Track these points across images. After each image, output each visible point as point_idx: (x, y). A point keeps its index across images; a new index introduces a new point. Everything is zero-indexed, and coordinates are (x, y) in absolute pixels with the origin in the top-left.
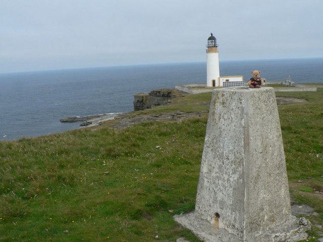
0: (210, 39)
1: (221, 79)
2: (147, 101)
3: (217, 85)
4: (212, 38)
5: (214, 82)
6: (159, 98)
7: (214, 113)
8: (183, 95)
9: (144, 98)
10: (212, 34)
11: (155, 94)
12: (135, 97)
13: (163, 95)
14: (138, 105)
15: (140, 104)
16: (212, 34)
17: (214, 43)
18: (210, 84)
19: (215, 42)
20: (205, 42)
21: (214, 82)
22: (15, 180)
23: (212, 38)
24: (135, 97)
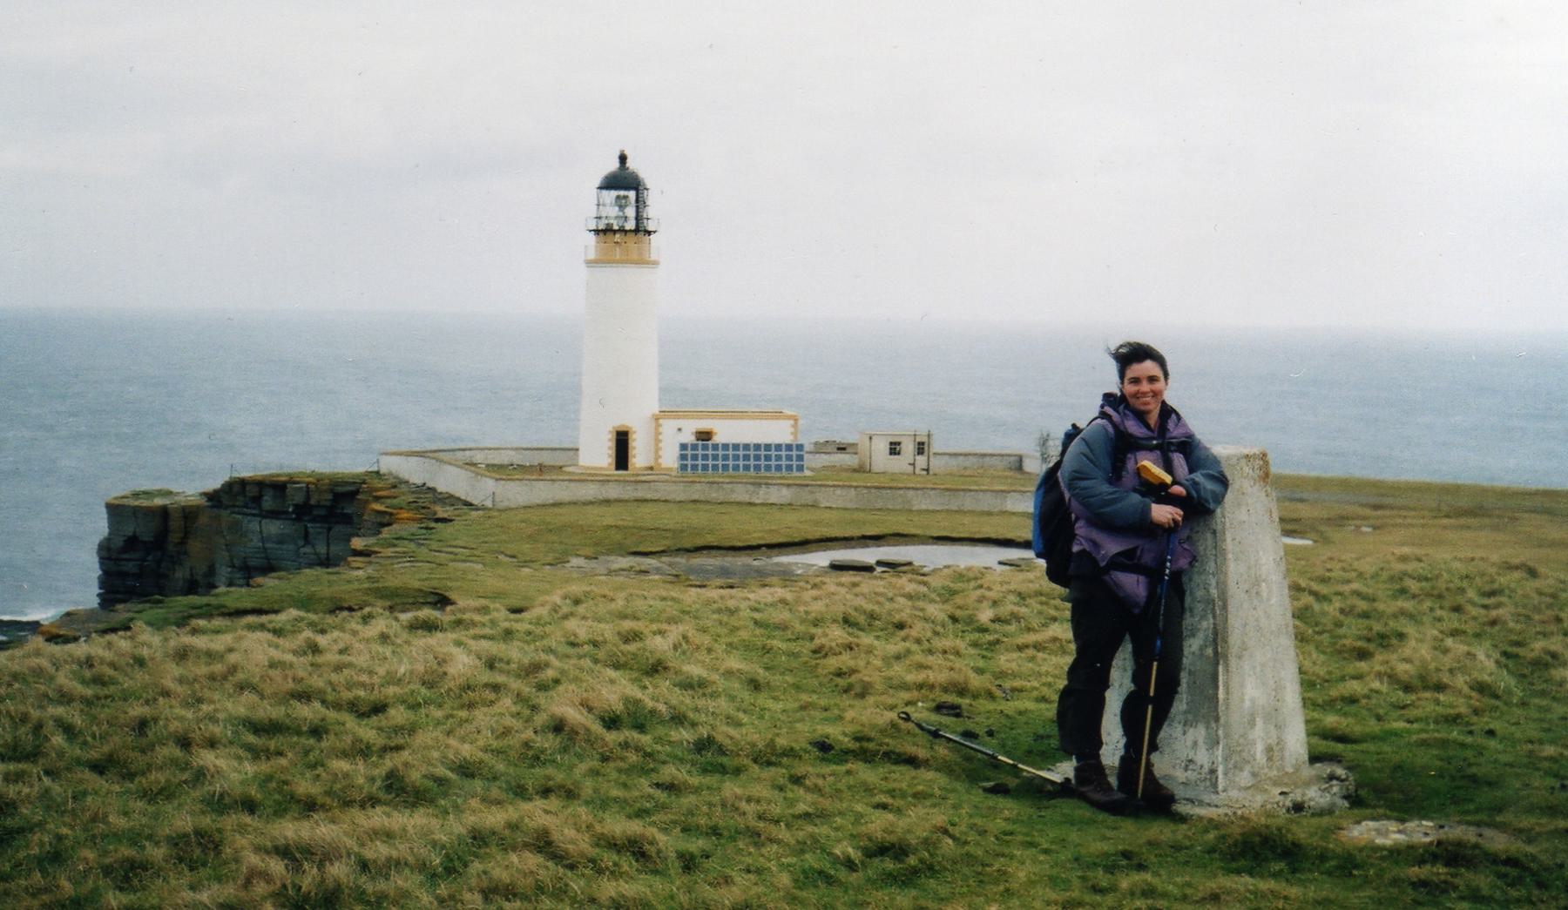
0: (611, 183)
1: (669, 426)
2: (195, 546)
3: (639, 457)
4: (622, 181)
5: (622, 441)
6: (273, 527)
7: (1267, 827)
8: (441, 512)
9: (176, 524)
10: (623, 159)
11: (245, 496)
12: (116, 511)
13: (303, 511)
14: (130, 567)
15: (155, 556)
16: (623, 159)
17: (631, 212)
18: (598, 455)
19: (640, 203)
20: (588, 203)
21: (622, 441)
22: (1322, 838)
23: (622, 181)
24: (116, 511)
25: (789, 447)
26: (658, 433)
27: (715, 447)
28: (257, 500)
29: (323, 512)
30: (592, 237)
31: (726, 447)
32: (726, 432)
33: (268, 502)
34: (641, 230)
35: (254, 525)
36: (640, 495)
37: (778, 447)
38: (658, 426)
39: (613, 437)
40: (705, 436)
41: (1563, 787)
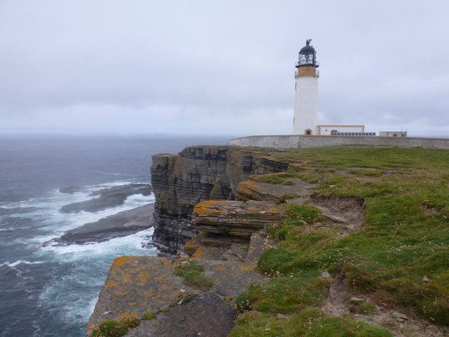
4: (308, 51)
6: (198, 162)
10: (308, 43)
19: (314, 58)
20: (295, 58)
23: (308, 51)
28: (194, 153)
29: (214, 157)
34: (314, 65)
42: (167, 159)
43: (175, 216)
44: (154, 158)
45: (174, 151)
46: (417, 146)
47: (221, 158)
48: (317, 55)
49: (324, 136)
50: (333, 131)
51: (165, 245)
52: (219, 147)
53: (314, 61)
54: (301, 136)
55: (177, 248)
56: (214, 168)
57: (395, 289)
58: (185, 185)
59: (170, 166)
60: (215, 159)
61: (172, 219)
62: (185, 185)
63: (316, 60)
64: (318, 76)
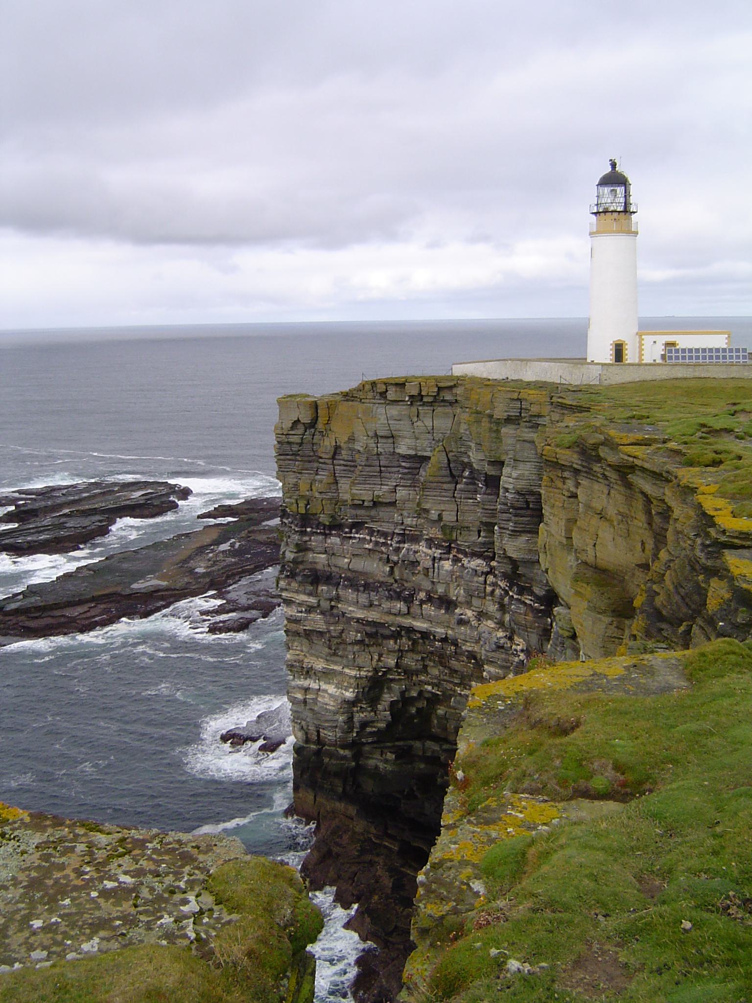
1: (648, 340)
2: (335, 426)
3: (630, 356)
4: (614, 179)
6: (394, 411)
10: (614, 165)
16: (614, 165)
18: (607, 356)
19: (627, 195)
20: (589, 194)
21: (619, 351)
23: (614, 179)
25: (724, 350)
26: (641, 345)
27: (677, 351)
28: (383, 394)
29: (430, 399)
30: (594, 216)
31: (684, 351)
32: (685, 342)
33: (391, 395)
34: (627, 211)
35: (381, 410)
36: (697, 374)
37: (717, 350)
38: (641, 340)
39: (613, 347)
40: (670, 345)
41: (282, 999)
42: (315, 406)
43: (335, 526)
44: (285, 402)
45: (328, 381)
46: (691, 468)
47: (444, 401)
48: (633, 190)
49: (646, 365)
50: (667, 344)
51: (310, 594)
52: (437, 379)
53: (627, 204)
54: (603, 365)
55: (338, 598)
56: (429, 423)
57: (499, 603)
58: (361, 460)
59: (321, 421)
60: (431, 404)
61: (326, 535)
62: (361, 460)
63: (632, 200)
64: (636, 233)
